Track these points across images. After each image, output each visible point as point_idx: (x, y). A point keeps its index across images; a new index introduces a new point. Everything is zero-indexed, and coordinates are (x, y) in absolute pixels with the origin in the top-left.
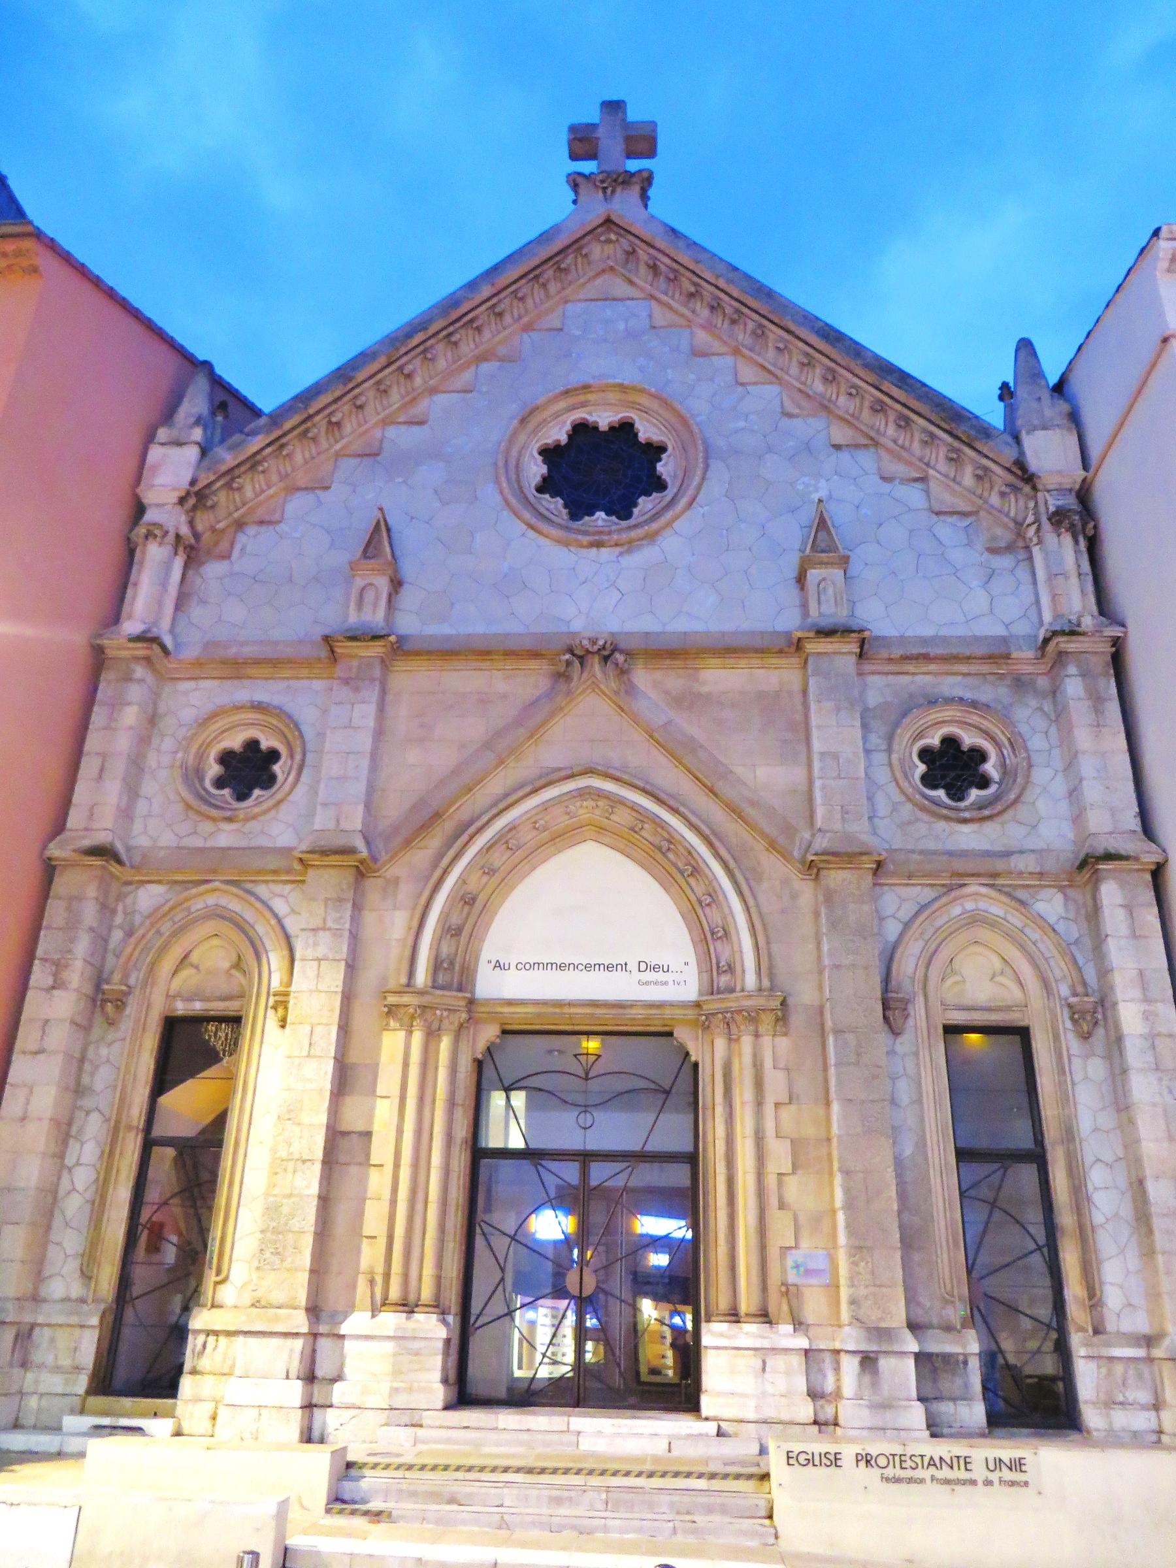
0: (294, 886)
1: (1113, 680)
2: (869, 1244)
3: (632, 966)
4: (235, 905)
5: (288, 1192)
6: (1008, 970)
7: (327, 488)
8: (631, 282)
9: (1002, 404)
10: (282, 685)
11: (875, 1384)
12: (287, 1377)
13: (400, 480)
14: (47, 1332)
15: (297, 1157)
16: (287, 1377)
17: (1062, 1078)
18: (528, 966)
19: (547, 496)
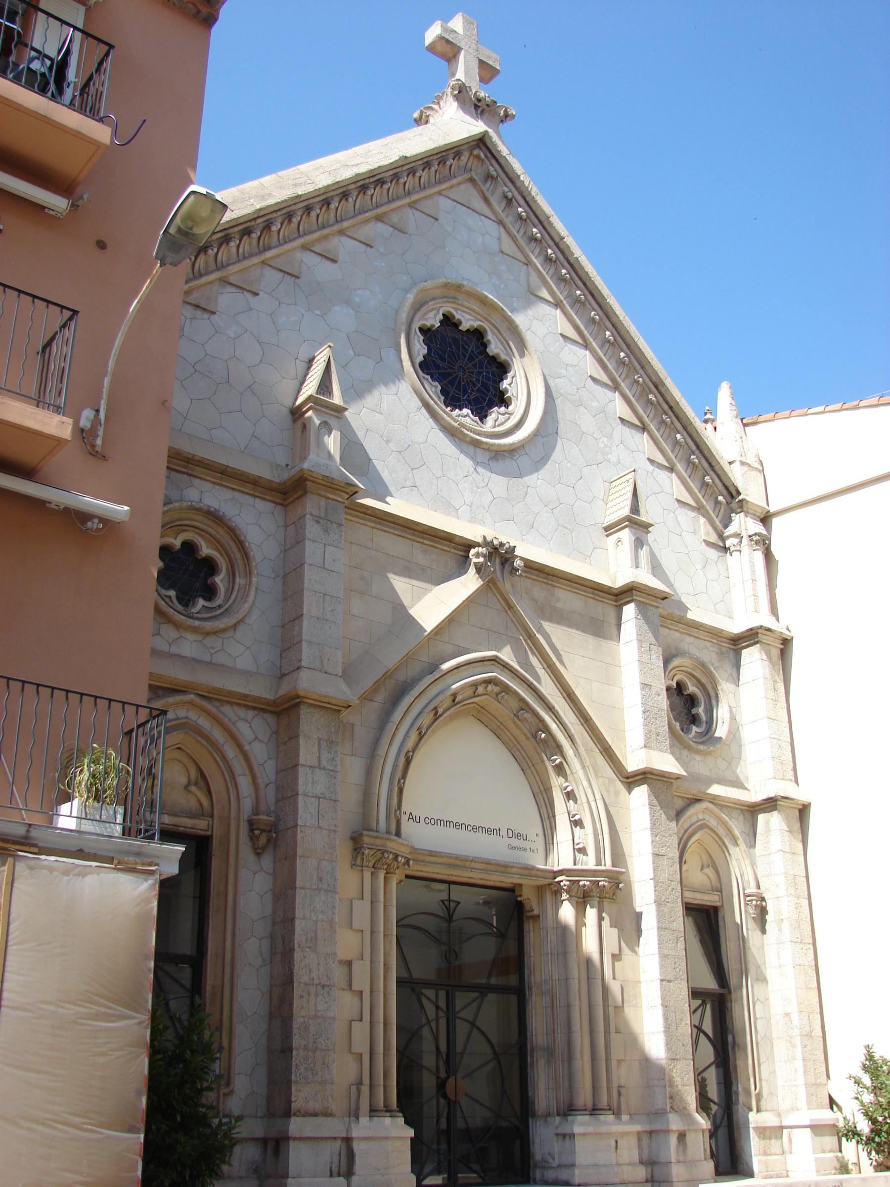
0: (256, 712)
1: (781, 667)
2: (678, 1057)
3: (503, 832)
4: (204, 723)
5: (312, 1013)
6: (202, 784)
7: (256, 294)
8: (486, 200)
9: (638, 910)
10: (228, 494)
11: (685, 1151)
12: (331, 1175)
13: (318, 312)
14: (578, 896)
15: (317, 981)
16: (331, 1175)
17: (60, 386)
18: (433, 822)
19: (422, 338)
